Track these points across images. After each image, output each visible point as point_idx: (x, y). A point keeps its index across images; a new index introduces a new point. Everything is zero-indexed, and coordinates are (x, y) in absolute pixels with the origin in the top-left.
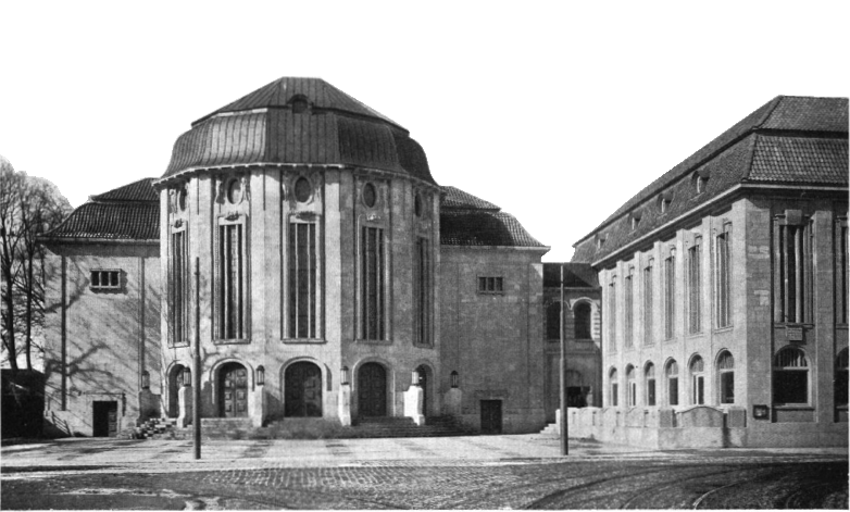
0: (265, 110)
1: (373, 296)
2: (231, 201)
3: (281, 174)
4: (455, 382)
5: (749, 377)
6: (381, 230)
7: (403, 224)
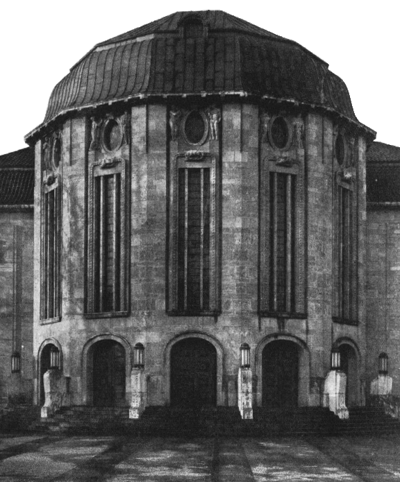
0: (151, 37)
1: (282, 285)
2: (110, 148)
3: (170, 104)
4: (383, 367)
5: (32, 329)
6: (294, 177)
7: (321, 167)
